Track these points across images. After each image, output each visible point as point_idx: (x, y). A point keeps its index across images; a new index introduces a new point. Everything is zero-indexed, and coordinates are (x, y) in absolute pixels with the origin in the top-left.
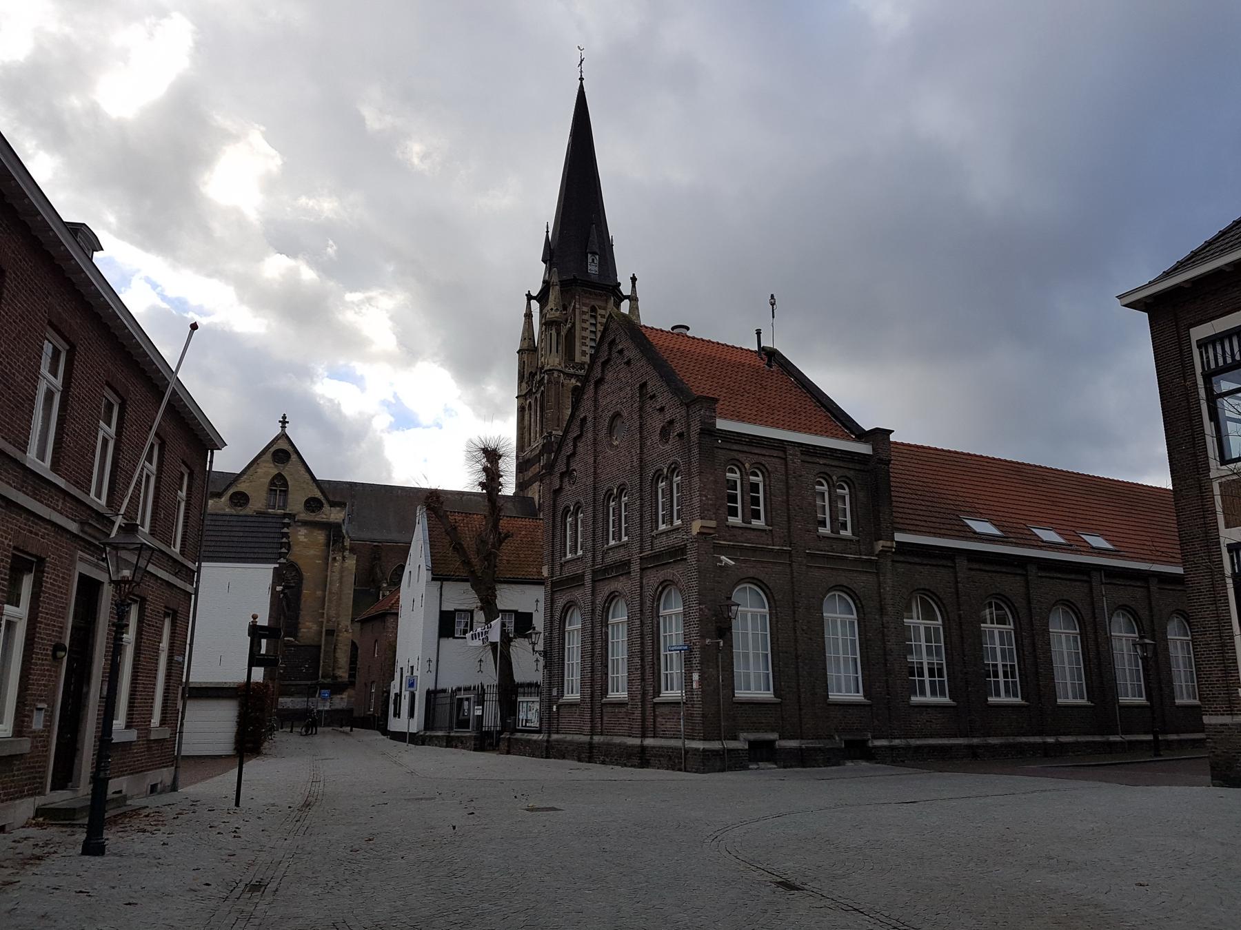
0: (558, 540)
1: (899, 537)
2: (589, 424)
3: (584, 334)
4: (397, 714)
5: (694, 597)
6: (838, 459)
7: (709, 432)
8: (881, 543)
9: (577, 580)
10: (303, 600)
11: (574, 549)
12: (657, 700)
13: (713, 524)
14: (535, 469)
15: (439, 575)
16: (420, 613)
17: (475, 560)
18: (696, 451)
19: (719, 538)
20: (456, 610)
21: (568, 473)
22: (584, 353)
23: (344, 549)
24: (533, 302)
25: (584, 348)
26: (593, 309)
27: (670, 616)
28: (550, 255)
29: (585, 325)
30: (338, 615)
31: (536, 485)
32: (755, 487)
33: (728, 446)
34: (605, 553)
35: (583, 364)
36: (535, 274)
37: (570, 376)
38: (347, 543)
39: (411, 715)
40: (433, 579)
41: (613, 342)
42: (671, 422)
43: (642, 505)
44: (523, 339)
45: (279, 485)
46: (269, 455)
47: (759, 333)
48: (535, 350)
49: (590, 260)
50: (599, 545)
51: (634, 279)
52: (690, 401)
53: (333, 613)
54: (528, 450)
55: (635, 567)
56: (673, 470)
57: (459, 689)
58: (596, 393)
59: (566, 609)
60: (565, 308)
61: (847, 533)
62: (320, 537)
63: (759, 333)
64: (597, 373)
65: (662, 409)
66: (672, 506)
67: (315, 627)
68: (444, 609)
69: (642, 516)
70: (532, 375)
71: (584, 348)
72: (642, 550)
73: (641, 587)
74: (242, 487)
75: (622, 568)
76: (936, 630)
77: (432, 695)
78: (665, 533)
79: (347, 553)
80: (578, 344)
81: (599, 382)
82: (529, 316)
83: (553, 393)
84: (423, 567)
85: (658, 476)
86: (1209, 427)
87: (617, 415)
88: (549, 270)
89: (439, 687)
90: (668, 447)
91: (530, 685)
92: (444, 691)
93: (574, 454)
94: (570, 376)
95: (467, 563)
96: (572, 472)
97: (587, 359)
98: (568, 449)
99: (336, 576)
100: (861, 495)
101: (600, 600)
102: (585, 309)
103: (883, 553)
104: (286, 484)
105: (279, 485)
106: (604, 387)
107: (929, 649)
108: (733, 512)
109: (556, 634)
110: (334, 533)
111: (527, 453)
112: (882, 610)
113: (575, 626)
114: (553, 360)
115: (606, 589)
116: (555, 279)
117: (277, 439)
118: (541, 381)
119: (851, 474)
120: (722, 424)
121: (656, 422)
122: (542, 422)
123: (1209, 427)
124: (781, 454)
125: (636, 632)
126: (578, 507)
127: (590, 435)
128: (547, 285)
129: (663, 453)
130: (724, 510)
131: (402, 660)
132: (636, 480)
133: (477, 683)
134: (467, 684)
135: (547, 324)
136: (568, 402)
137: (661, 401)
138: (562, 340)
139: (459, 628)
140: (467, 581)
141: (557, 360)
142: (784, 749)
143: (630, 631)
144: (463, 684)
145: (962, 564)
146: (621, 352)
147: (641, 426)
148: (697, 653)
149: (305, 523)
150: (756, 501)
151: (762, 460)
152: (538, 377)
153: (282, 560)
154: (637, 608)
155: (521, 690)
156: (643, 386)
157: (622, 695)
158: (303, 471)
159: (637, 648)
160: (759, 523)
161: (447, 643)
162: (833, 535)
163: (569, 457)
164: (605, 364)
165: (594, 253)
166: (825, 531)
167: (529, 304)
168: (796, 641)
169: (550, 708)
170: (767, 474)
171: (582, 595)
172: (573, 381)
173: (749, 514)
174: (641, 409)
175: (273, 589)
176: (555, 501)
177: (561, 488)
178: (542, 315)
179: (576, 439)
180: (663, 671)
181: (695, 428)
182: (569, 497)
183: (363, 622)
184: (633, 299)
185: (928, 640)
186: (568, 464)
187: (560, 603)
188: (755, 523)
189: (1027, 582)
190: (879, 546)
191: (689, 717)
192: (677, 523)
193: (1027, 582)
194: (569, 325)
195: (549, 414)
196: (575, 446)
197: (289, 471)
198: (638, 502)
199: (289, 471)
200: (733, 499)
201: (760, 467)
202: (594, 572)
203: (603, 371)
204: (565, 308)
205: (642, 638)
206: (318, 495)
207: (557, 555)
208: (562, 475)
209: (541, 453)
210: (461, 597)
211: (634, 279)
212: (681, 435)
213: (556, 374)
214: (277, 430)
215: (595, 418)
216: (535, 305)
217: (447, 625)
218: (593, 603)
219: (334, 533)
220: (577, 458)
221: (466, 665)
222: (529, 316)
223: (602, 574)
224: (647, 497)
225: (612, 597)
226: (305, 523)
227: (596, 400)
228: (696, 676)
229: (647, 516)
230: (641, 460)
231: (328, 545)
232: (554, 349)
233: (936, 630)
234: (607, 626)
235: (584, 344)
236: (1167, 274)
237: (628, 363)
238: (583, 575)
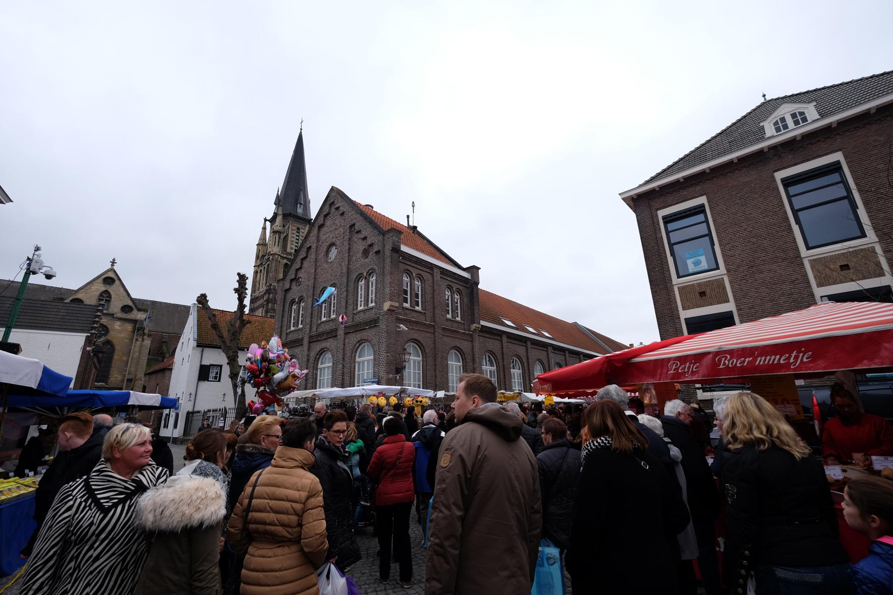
0: (285, 319)
1: (483, 323)
2: (313, 250)
4: (166, 426)
5: (383, 347)
6: (456, 279)
7: (396, 250)
8: (475, 325)
10: (114, 361)
13: (397, 304)
14: (261, 302)
15: (202, 344)
16: (187, 365)
17: (225, 334)
18: (388, 261)
19: (399, 313)
20: (211, 365)
22: (292, 248)
23: (144, 334)
24: (268, 223)
26: (298, 229)
27: (363, 362)
28: (278, 202)
30: (136, 371)
31: (260, 310)
34: (319, 325)
35: (290, 254)
36: (270, 210)
37: (283, 258)
38: (146, 331)
39: (175, 426)
41: (332, 204)
42: (371, 245)
43: (347, 295)
44: (261, 239)
45: (106, 296)
46: (101, 279)
47: (408, 217)
48: (266, 245)
50: (314, 320)
53: (133, 369)
54: (257, 292)
57: (209, 411)
60: (284, 226)
61: (458, 319)
62: (129, 327)
63: (408, 217)
65: (365, 238)
67: (120, 377)
69: (347, 302)
70: (263, 256)
74: (79, 296)
75: (332, 334)
79: (145, 337)
82: (264, 228)
83: (274, 264)
84: (192, 339)
85: (359, 277)
86: (670, 259)
88: (277, 208)
89: (196, 410)
90: (367, 260)
92: (199, 412)
93: (300, 268)
94: (283, 258)
97: (293, 251)
98: (297, 265)
99: (137, 349)
100: (465, 299)
101: (313, 354)
103: (475, 331)
104: (110, 296)
105: (106, 296)
106: (324, 229)
110: (138, 328)
111: (257, 294)
112: (474, 360)
114: (276, 250)
115: (317, 347)
116: (280, 212)
117: (108, 271)
118: (268, 259)
119: (461, 288)
120: (404, 248)
121: (360, 246)
123: (670, 259)
125: (339, 372)
126: (301, 299)
127: (312, 256)
128: (275, 215)
129: (361, 264)
130: (401, 298)
132: (344, 280)
133: (221, 406)
134: (215, 408)
135: (274, 232)
136: (281, 270)
137: (364, 233)
138: (281, 241)
139: (212, 375)
140: (220, 348)
144: (211, 408)
146: (337, 208)
149: (120, 319)
152: (266, 257)
153: (93, 331)
158: (122, 290)
160: (419, 308)
161: (204, 385)
163: (297, 270)
164: (326, 216)
166: (449, 316)
167: (265, 223)
168: (436, 376)
173: (414, 303)
175: (84, 348)
176: (285, 296)
177: (290, 289)
179: (303, 259)
181: (389, 247)
183: (150, 374)
186: (296, 274)
188: (417, 308)
189: (527, 349)
190: (474, 326)
193: (527, 349)
195: (271, 275)
196: (302, 263)
197: (113, 289)
198: (345, 294)
199: (113, 289)
201: (420, 277)
202: (310, 337)
204: (284, 226)
206: (131, 304)
207: (284, 328)
208: (292, 280)
209: (265, 294)
212: (378, 252)
214: (109, 267)
216: (268, 224)
217: (204, 373)
218: (308, 356)
219: (138, 328)
220: (302, 270)
221: (217, 396)
222: (264, 228)
224: (351, 290)
225: (322, 352)
226: (120, 319)
227: (318, 237)
229: (350, 302)
230: (348, 269)
231: (134, 332)
236: (647, 182)
237: (342, 214)
238: (302, 339)
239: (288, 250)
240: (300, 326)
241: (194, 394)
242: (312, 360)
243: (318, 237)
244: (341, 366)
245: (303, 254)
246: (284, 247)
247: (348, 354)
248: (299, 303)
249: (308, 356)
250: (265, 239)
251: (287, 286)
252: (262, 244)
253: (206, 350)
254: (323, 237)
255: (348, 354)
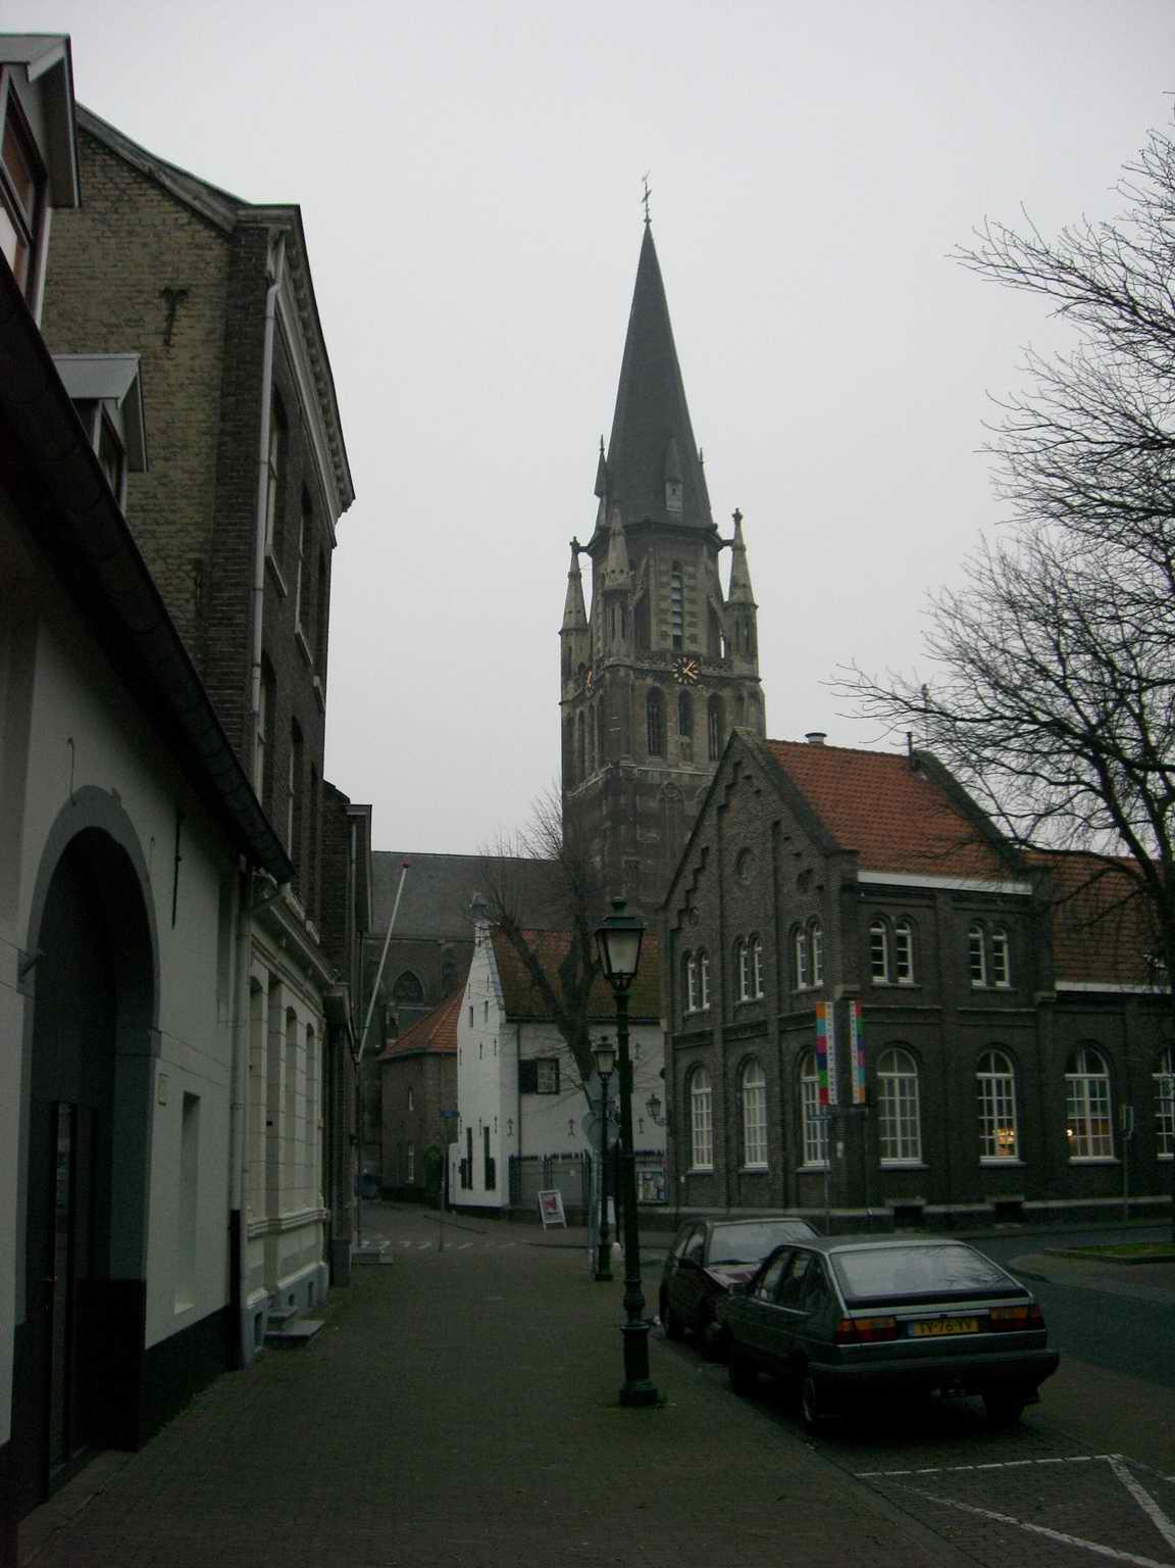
0: (678, 990)
2: (713, 856)
3: (664, 592)
4: (467, 1183)
7: (851, 887)
9: (703, 1038)
11: (698, 1002)
12: (800, 1169)
15: (517, 1016)
21: (686, 911)
22: (664, 635)
25: (664, 628)
26: (676, 566)
28: (610, 481)
29: (664, 592)
32: (902, 941)
33: (872, 899)
36: (583, 516)
40: (508, 1021)
41: (738, 764)
42: (809, 871)
43: (778, 961)
44: (568, 613)
49: (669, 491)
51: (738, 517)
52: (831, 853)
55: (773, 1029)
56: (813, 924)
58: (720, 820)
59: (692, 1070)
64: (720, 797)
65: (798, 855)
66: (812, 964)
68: (524, 1058)
71: (664, 628)
72: (780, 1010)
73: (780, 1052)
76: (1102, 1084)
77: (515, 1162)
78: (805, 993)
80: (654, 621)
81: (723, 808)
82: (575, 576)
84: (493, 1002)
85: (796, 929)
87: (745, 851)
88: (606, 509)
91: (649, 1153)
92: (534, 1158)
93: (694, 890)
95: (549, 998)
96: (692, 910)
98: (686, 882)
101: (733, 1061)
102: (663, 567)
106: (729, 817)
107: (1093, 1105)
108: (878, 971)
109: (680, 1098)
113: (702, 1090)
114: (621, 650)
115: (737, 1053)
116: (617, 525)
120: (866, 877)
121: (791, 869)
122: (602, 744)
124: (930, 903)
127: (713, 869)
131: (298, 1065)
132: (772, 930)
138: (631, 619)
141: (623, 650)
142: (934, 1216)
143: (768, 1100)
144: (559, 1151)
145: (1131, 1008)
146: (748, 778)
147: (776, 870)
148: (841, 1124)
150: (903, 956)
151: (910, 911)
154: (776, 1072)
155: (637, 1159)
156: (777, 824)
157: (761, 1164)
159: (777, 1116)
160: (906, 981)
161: (532, 1102)
162: (990, 988)
165: (675, 481)
166: (978, 983)
167: (575, 560)
169: (678, 1179)
170: (914, 925)
171: (713, 1056)
172: (649, 681)
174: (775, 849)
176: (672, 942)
177: (679, 929)
178: (598, 577)
179: (698, 872)
180: (806, 1140)
181: (835, 885)
182: (690, 938)
184: (738, 548)
185: (1093, 1094)
186: (687, 900)
187: (684, 1062)
191: (832, 1186)
192: (819, 983)
194: (639, 594)
196: (696, 879)
200: (878, 955)
202: (725, 1031)
203: (727, 795)
204: (633, 566)
205: (783, 1106)
207: (678, 1007)
208: (681, 912)
210: (546, 1041)
211: (738, 517)
212: (820, 888)
213: (622, 673)
215: (720, 851)
216: (585, 560)
217: (528, 1078)
218: (725, 1065)
220: (699, 894)
223: (731, 1035)
227: (719, 829)
228: (840, 1146)
232: (619, 633)
233: (1102, 1084)
234: (741, 1091)
235: (663, 621)
238: (711, 1033)
239: (655, 645)
240: (706, 1006)
241: (515, 1120)
242: (731, 1074)
243: (719, 829)
244: (777, 1089)
245: (694, 862)
246: (641, 640)
247: (789, 1069)
248: (698, 960)
249: (725, 1065)
250: (581, 610)
251: (675, 925)
252: (574, 630)
253: (528, 1030)
254: (729, 832)
255: (789, 1069)
